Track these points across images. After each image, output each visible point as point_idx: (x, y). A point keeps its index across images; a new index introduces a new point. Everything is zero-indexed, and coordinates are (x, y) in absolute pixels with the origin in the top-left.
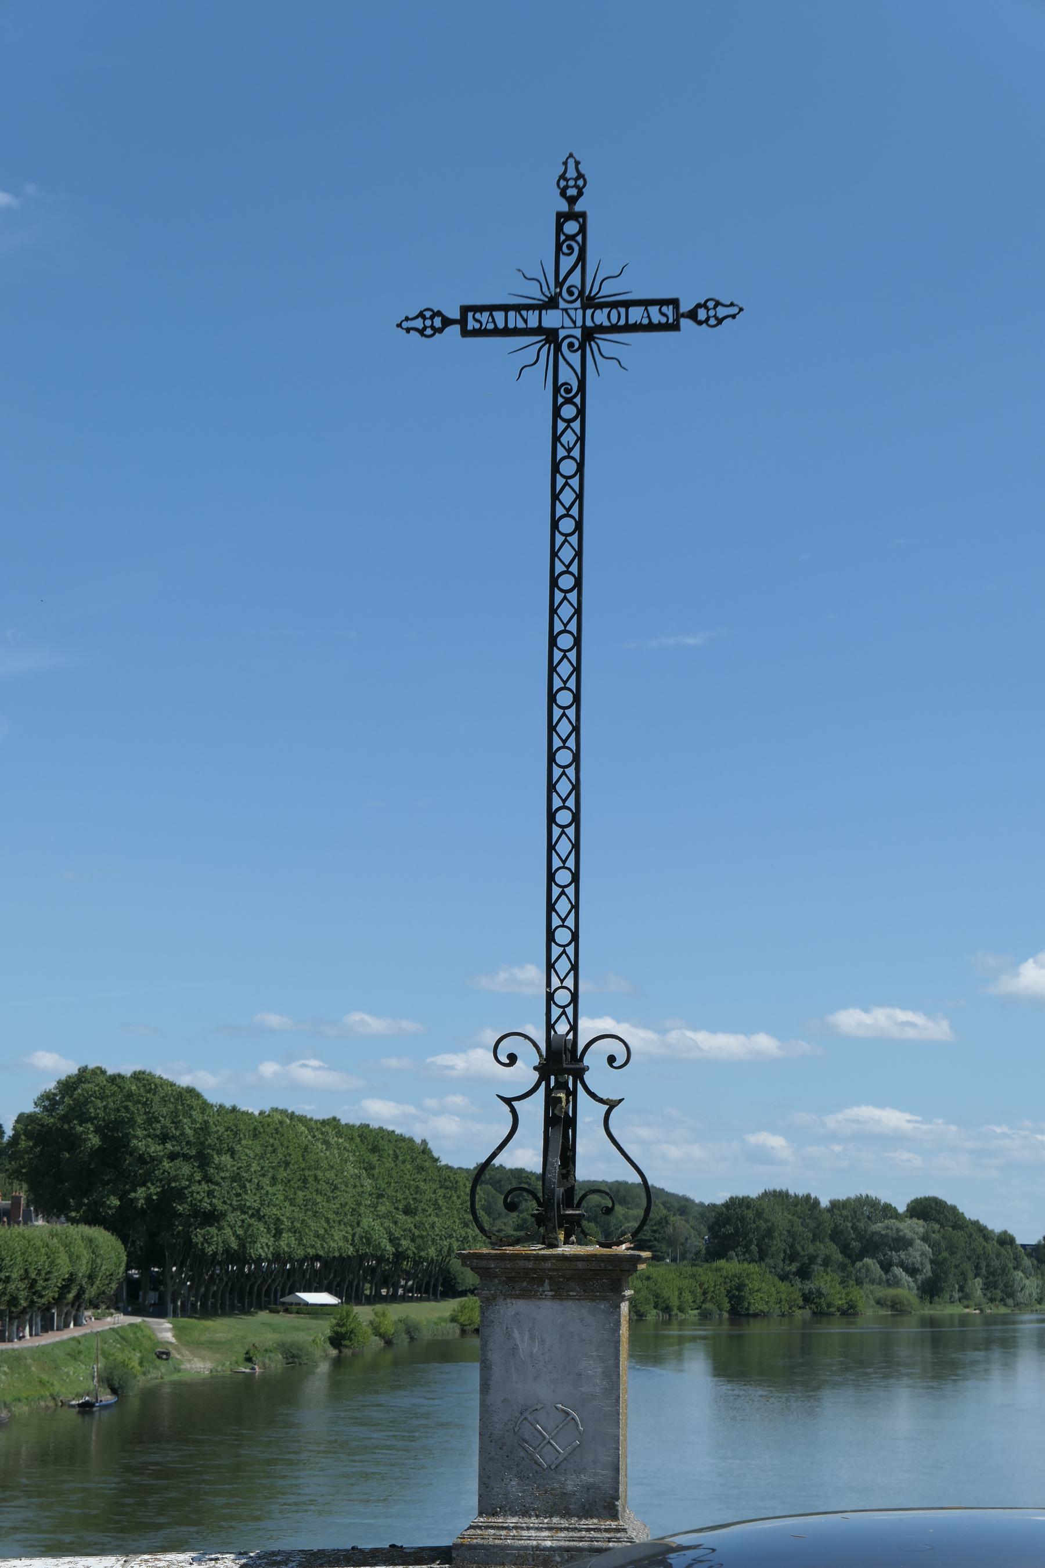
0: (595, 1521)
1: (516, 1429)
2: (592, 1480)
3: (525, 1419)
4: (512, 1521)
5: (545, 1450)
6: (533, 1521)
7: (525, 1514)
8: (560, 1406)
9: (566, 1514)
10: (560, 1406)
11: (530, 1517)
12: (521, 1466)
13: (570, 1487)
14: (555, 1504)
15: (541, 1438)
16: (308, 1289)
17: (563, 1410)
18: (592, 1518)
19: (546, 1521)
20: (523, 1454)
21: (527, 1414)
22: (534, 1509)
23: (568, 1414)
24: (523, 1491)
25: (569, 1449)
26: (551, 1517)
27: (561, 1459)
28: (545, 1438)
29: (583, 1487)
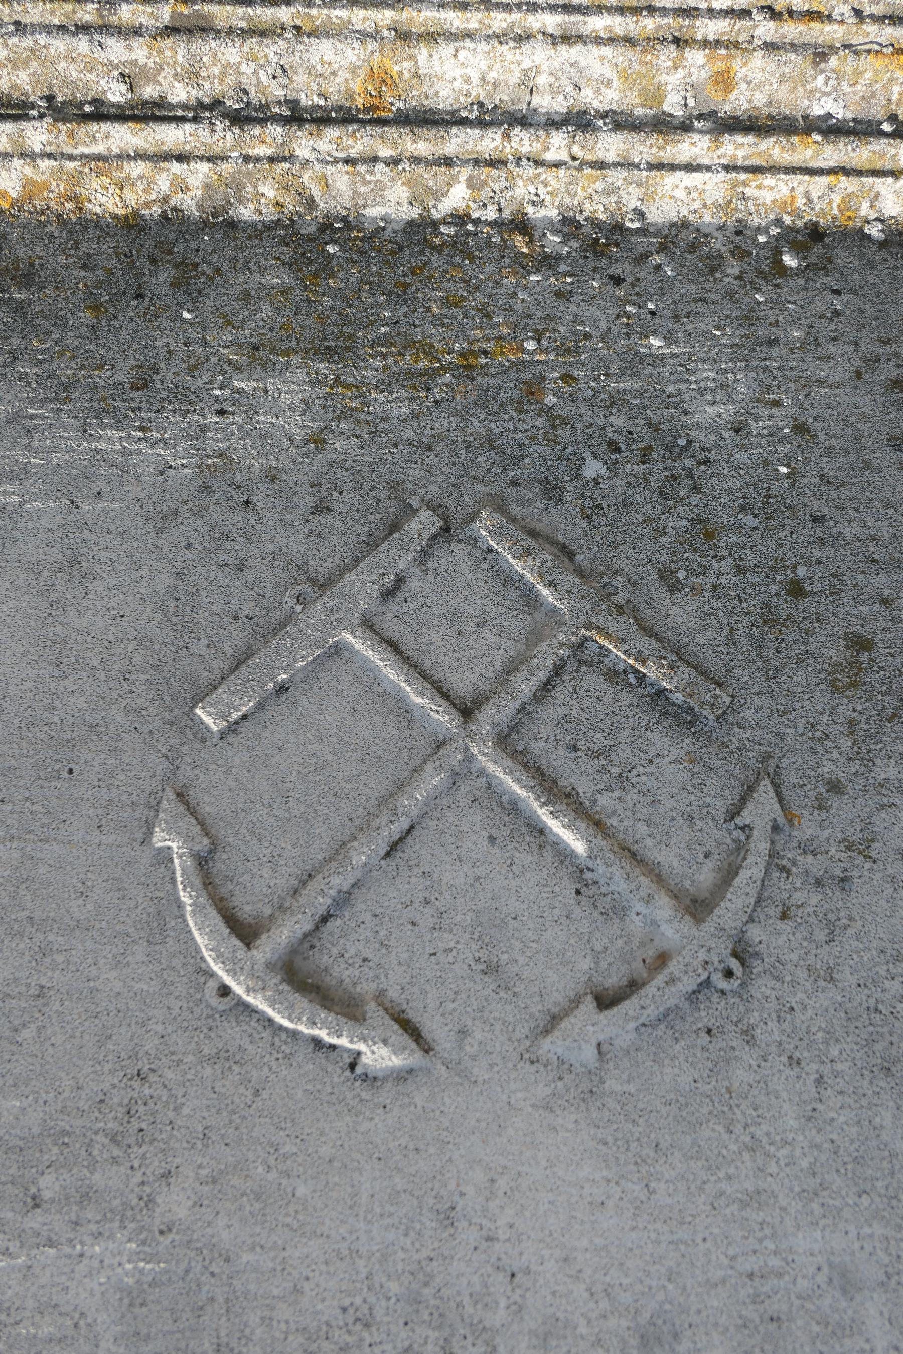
0: (104, 199)
1: (763, 809)
2: (110, 439)
3: (697, 907)
4: (689, 190)
5: (496, 648)
6: (549, 187)
7: (602, 243)
8: (379, 1056)
9: (314, 243)
10: (379, 1056)
11: (569, 225)
12: (676, 523)
13: (287, 398)
14: (400, 294)
15: (542, 739)
16: (573, 854)
17: (345, 1006)
18: (132, 224)
19: (457, 197)
20: (679, 614)
21: (695, 948)
22: (547, 262)
23: (299, 977)
24: (635, 362)
25: (290, 657)
26: (420, 230)
27: (362, 586)
28: (506, 741)
29: (184, 399)
